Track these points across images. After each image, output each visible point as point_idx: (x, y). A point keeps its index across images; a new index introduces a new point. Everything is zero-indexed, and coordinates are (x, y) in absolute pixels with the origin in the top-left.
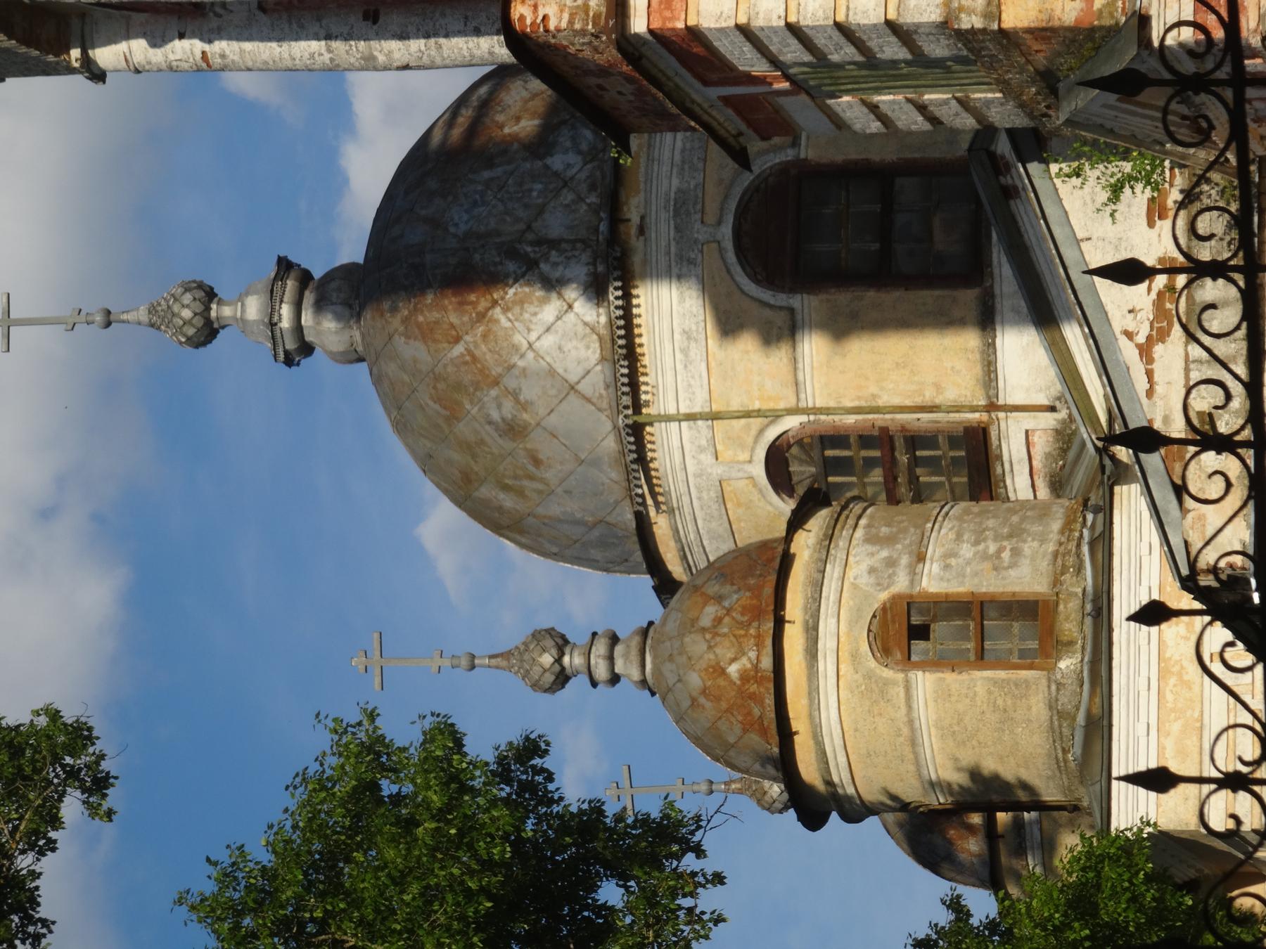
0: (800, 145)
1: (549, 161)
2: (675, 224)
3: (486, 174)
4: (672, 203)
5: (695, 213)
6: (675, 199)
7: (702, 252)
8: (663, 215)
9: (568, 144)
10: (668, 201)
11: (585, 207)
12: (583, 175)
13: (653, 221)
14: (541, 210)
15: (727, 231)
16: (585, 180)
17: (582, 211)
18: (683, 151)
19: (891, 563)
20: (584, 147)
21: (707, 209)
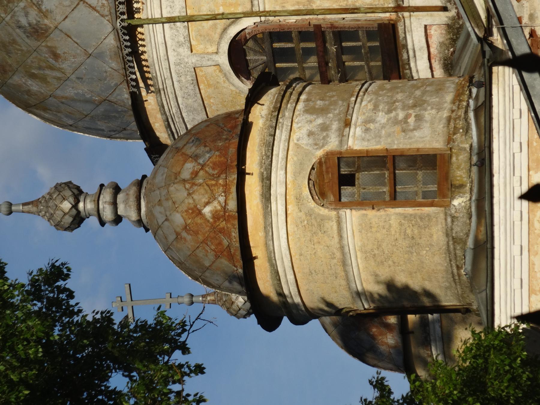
19: (325, 128)
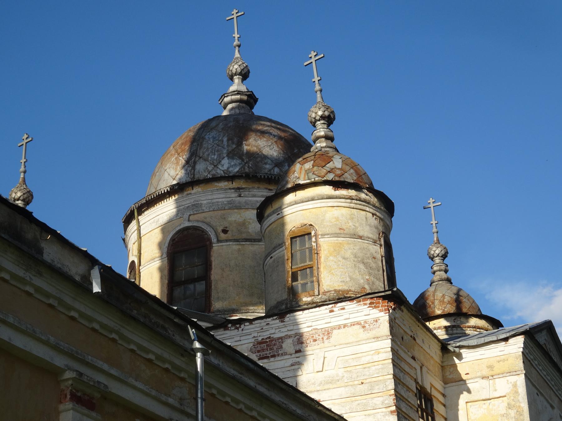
0: (218, 243)
1: (226, 158)
2: (190, 206)
3: (225, 139)
4: (197, 203)
5: (193, 212)
6: (198, 204)
7: (180, 218)
8: (192, 201)
9: (232, 163)
10: (197, 201)
11: (206, 175)
12: (219, 171)
13: (189, 198)
14: (206, 160)
15: (187, 224)
16: (216, 172)
17: (205, 174)
18: (218, 202)
20: (231, 169)
21: (195, 216)
